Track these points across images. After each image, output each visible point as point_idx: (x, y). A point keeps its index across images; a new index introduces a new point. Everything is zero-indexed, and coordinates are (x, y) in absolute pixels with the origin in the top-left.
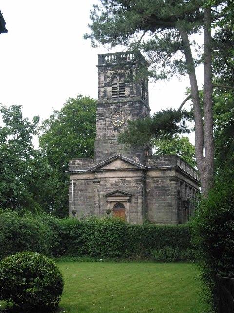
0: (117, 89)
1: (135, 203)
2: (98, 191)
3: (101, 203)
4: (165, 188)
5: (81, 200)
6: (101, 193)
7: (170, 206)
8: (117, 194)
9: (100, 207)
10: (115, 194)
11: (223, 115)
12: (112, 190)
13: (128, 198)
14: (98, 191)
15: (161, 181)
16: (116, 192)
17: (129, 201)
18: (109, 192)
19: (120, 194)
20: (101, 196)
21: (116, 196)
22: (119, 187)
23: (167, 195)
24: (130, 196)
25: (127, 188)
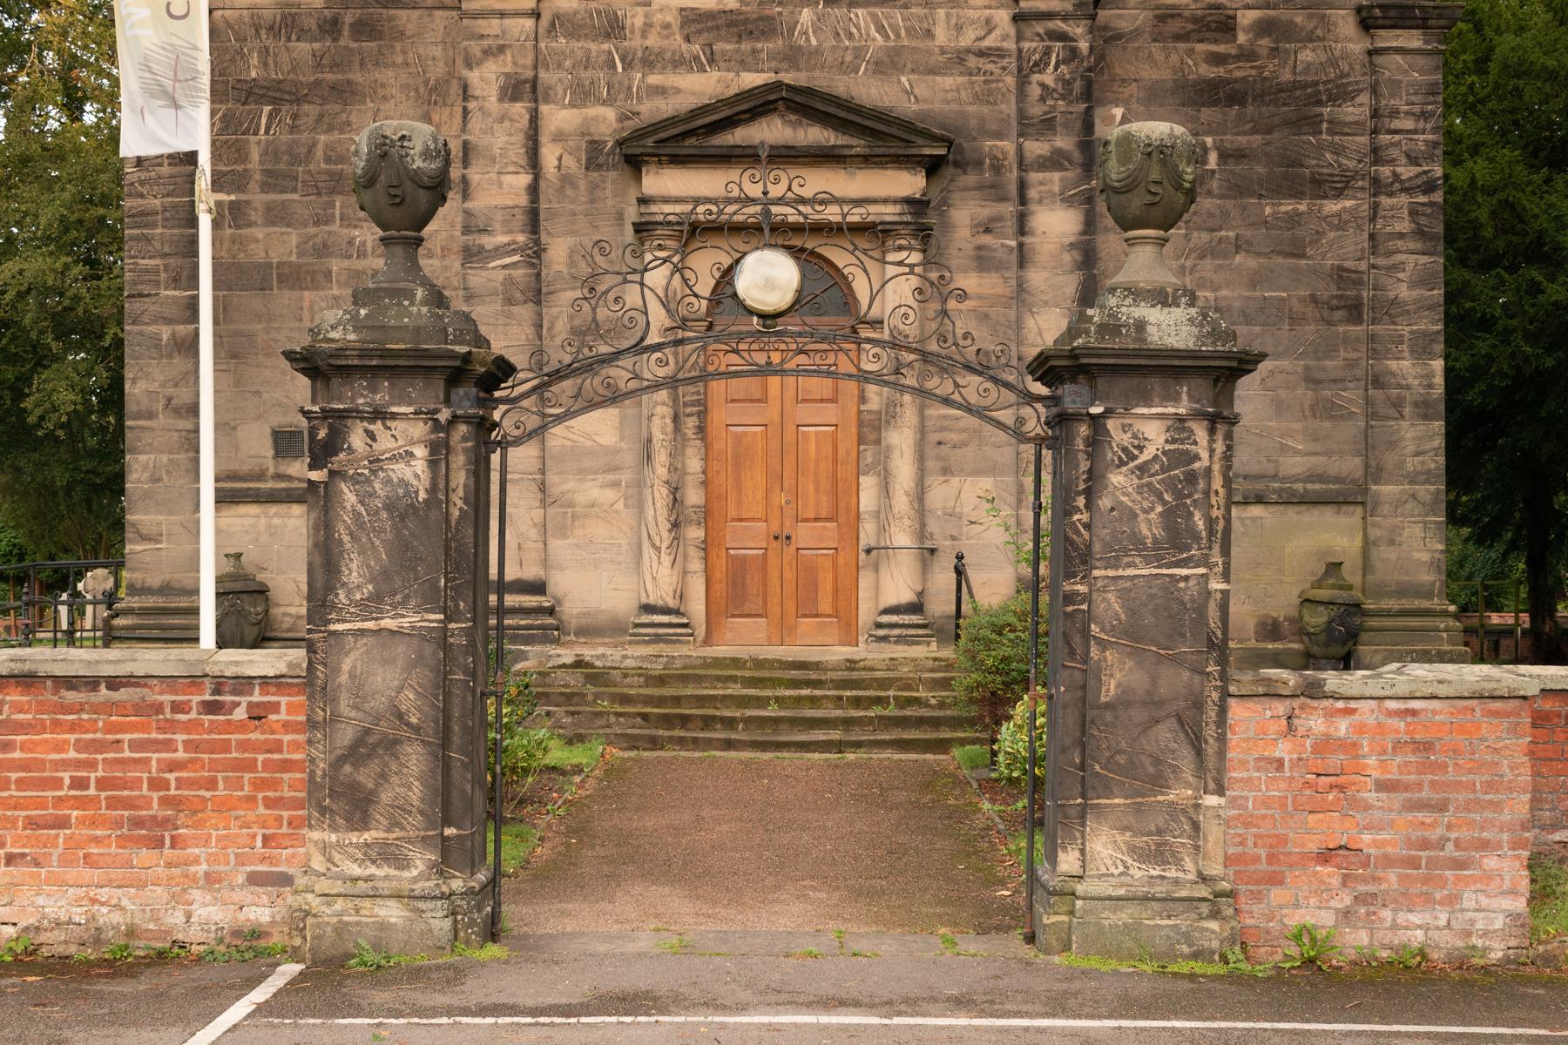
0: (87, 788)
1: (983, 261)
2: (514, 89)
3: (558, 251)
4: (1304, 105)
5: (277, 216)
6: (559, 117)
7: (1354, 312)
8: (772, 131)
9: (537, 294)
10: (740, 136)
11: (1205, 236)
12: (700, 86)
13: (910, 183)
14: (514, 89)
15: (1264, 28)
16: (758, 105)
17: (921, 223)
18: (665, 108)
19: (815, 135)
20: (550, 155)
21: (745, 157)
22: (793, 56)
23: (1322, 187)
24: (933, 167)
25: (888, 64)
